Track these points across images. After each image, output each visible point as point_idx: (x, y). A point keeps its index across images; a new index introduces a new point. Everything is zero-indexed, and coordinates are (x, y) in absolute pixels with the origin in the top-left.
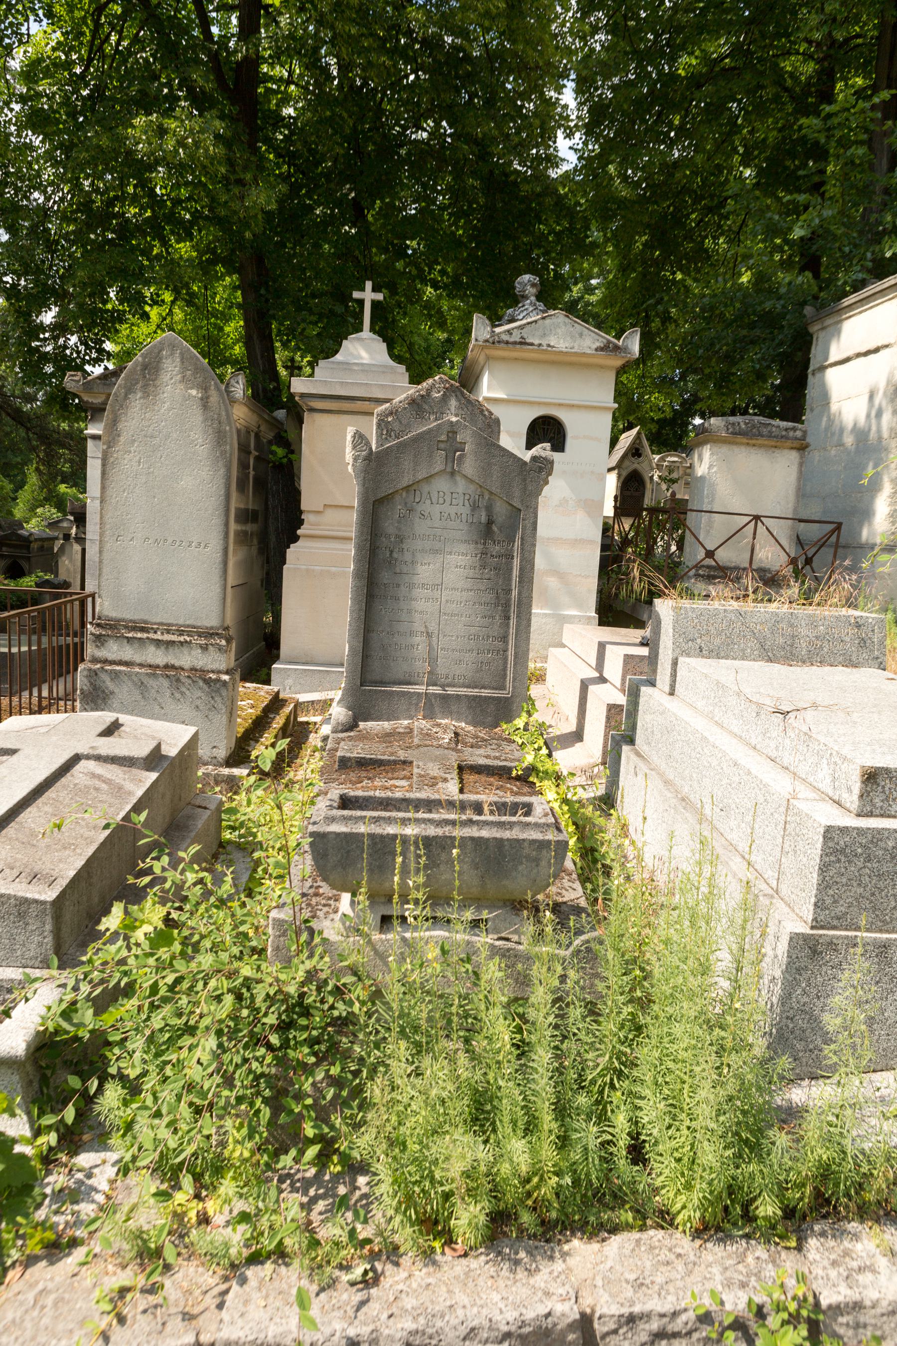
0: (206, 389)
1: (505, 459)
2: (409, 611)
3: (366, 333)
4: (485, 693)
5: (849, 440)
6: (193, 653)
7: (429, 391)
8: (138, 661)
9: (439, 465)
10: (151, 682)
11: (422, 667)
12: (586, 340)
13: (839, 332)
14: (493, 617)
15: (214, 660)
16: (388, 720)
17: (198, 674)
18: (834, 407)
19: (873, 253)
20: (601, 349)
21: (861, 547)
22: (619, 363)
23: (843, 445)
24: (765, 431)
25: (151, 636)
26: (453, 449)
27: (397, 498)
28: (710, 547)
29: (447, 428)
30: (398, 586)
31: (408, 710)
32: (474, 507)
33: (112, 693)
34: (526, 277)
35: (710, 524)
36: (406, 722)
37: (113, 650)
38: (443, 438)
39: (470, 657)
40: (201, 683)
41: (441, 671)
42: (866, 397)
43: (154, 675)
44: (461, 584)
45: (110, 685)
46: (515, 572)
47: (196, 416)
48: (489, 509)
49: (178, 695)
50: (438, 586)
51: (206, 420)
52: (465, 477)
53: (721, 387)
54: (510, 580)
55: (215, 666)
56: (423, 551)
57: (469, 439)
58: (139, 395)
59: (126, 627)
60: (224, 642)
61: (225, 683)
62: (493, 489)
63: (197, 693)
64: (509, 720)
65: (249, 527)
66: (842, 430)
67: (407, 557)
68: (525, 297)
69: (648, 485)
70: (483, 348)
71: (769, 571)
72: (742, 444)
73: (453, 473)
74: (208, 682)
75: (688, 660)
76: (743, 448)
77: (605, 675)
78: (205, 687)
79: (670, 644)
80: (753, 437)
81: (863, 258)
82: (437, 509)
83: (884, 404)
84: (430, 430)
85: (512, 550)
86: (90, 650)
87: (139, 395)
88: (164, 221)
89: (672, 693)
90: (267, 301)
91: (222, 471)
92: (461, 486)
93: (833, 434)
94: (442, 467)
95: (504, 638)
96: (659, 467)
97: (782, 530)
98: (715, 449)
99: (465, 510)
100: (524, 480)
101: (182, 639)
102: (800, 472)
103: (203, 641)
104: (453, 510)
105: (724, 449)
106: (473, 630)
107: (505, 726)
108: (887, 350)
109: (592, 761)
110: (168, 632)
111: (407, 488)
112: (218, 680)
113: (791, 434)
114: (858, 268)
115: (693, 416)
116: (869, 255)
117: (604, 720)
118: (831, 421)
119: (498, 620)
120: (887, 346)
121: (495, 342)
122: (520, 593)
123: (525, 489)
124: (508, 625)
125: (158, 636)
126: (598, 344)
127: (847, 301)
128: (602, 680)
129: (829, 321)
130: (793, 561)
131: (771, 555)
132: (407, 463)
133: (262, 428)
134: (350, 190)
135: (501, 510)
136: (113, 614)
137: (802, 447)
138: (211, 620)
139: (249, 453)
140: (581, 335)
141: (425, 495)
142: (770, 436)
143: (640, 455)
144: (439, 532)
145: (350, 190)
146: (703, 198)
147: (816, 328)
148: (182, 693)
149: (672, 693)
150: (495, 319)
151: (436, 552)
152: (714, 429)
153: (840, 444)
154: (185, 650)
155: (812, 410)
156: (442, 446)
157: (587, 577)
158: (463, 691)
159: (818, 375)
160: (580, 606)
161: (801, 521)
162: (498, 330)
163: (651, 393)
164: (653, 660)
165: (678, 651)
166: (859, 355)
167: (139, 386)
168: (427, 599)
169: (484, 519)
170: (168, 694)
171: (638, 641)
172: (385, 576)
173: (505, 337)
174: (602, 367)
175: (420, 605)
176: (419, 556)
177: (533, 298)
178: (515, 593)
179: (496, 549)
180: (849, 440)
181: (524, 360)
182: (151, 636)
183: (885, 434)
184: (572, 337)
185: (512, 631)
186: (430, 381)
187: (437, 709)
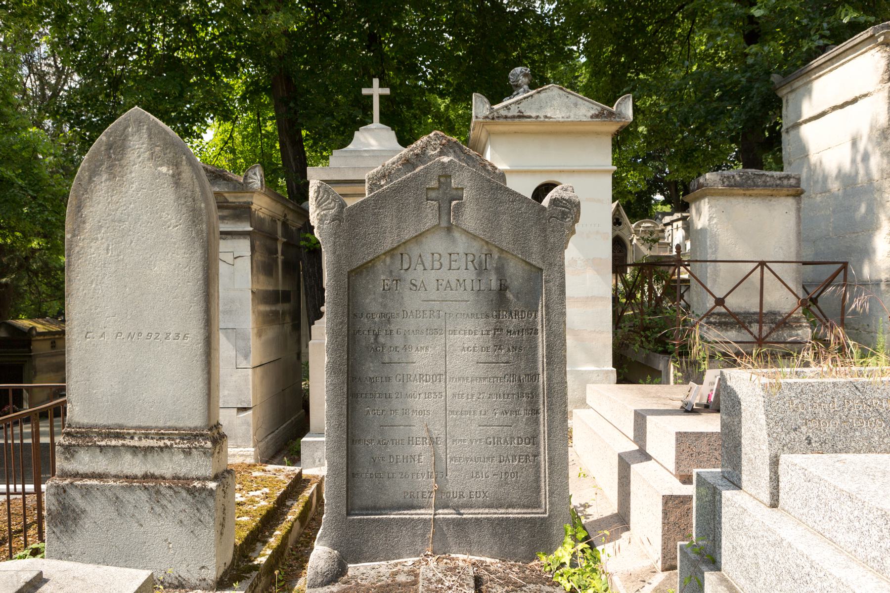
0: (177, 165)
1: (516, 205)
2: (405, 412)
3: (376, 124)
4: (514, 513)
5: (835, 186)
6: (175, 458)
7: (424, 149)
8: (113, 472)
9: (430, 219)
10: (128, 497)
11: (426, 484)
12: (584, 109)
13: (809, 92)
14: (517, 412)
15: (198, 466)
16: (387, 559)
17: (181, 483)
18: (813, 158)
19: (828, 23)
20: (597, 116)
21: (865, 284)
22: (614, 128)
23: (829, 191)
24: (759, 181)
25: (128, 442)
26: (448, 200)
27: (380, 266)
28: (720, 295)
29: (437, 171)
30: (388, 379)
31: (412, 543)
32: (481, 270)
33: (84, 512)
34: (518, 69)
35: (716, 273)
36: (410, 561)
37: (85, 461)
38: (434, 184)
39: (489, 467)
40: (184, 494)
41: (452, 488)
42: (849, 145)
43: (130, 487)
44: (470, 371)
45: (80, 502)
46: (542, 351)
47: (168, 195)
48: (500, 270)
49: (158, 510)
50: (440, 376)
51: (179, 198)
52: (466, 232)
53: (686, 161)
54: (535, 361)
55: (201, 472)
56: (418, 331)
57: (467, 183)
58: (105, 176)
59: (99, 434)
60: (209, 444)
61: (211, 492)
62: (504, 245)
63: (180, 505)
64: (549, 551)
65: (279, 307)
66: (825, 178)
67: (398, 341)
68: (518, 86)
69: (629, 247)
70: (484, 124)
71: (779, 313)
72: (739, 195)
73: (449, 229)
74: (192, 492)
75: (798, 459)
76: (740, 199)
77: (649, 450)
78: (189, 498)
79: (763, 435)
80: (749, 187)
81: (820, 28)
82: (432, 275)
83: (870, 148)
84: (417, 176)
85: (534, 322)
86: (60, 463)
87: (105, 176)
88: (215, 62)
89: (774, 505)
90: (296, 113)
91: (199, 253)
92: (462, 244)
93: (816, 182)
94: (435, 222)
95: (534, 439)
96: (637, 232)
97: (788, 273)
98: (713, 202)
99: (469, 275)
100: (544, 230)
101: (161, 443)
102: (799, 218)
103: (186, 445)
104: (453, 276)
105: (722, 202)
106: (491, 431)
107: (544, 559)
108: (867, 99)
109: (647, 563)
110: (147, 436)
111: (391, 252)
112: (204, 489)
113: (785, 182)
114: (818, 37)
115: (654, 193)
116: (825, 25)
117: (660, 515)
118: (812, 170)
119: (523, 416)
120: (865, 95)
121: (494, 118)
122: (549, 379)
123: (545, 241)
124: (537, 422)
125: (135, 442)
126: (593, 112)
127: (815, 63)
128: (643, 455)
129: (797, 84)
130: (803, 303)
131: (781, 299)
132: (388, 221)
133: (289, 217)
134: (365, 22)
135: (515, 270)
136: (85, 421)
137: (797, 194)
138: (221, 411)
139: (277, 239)
140: (576, 105)
141: (415, 259)
142: (765, 185)
143: (620, 224)
144: (436, 306)
145: (365, 22)
146: (656, 12)
147: (785, 92)
148: (163, 507)
149: (774, 505)
150: (494, 99)
151: (435, 331)
152: (710, 183)
153: (825, 191)
154: (166, 456)
155: (790, 164)
156: (433, 194)
157: (602, 332)
158: (483, 513)
159: (792, 133)
160: (596, 362)
161: (805, 263)
162: (496, 107)
163: (628, 171)
164: (729, 445)
165: (777, 445)
166: (834, 108)
167: (104, 167)
168: (428, 395)
169: (494, 284)
170: (147, 508)
171: (678, 405)
172: (370, 368)
173: (504, 113)
174: (597, 133)
175: (418, 403)
176: (412, 337)
177: (526, 87)
178: (542, 378)
179: (513, 323)
180: (835, 186)
181: (523, 133)
182: (128, 442)
183: (876, 175)
184: (568, 107)
185: (543, 428)
186: (425, 138)
187: (450, 540)
